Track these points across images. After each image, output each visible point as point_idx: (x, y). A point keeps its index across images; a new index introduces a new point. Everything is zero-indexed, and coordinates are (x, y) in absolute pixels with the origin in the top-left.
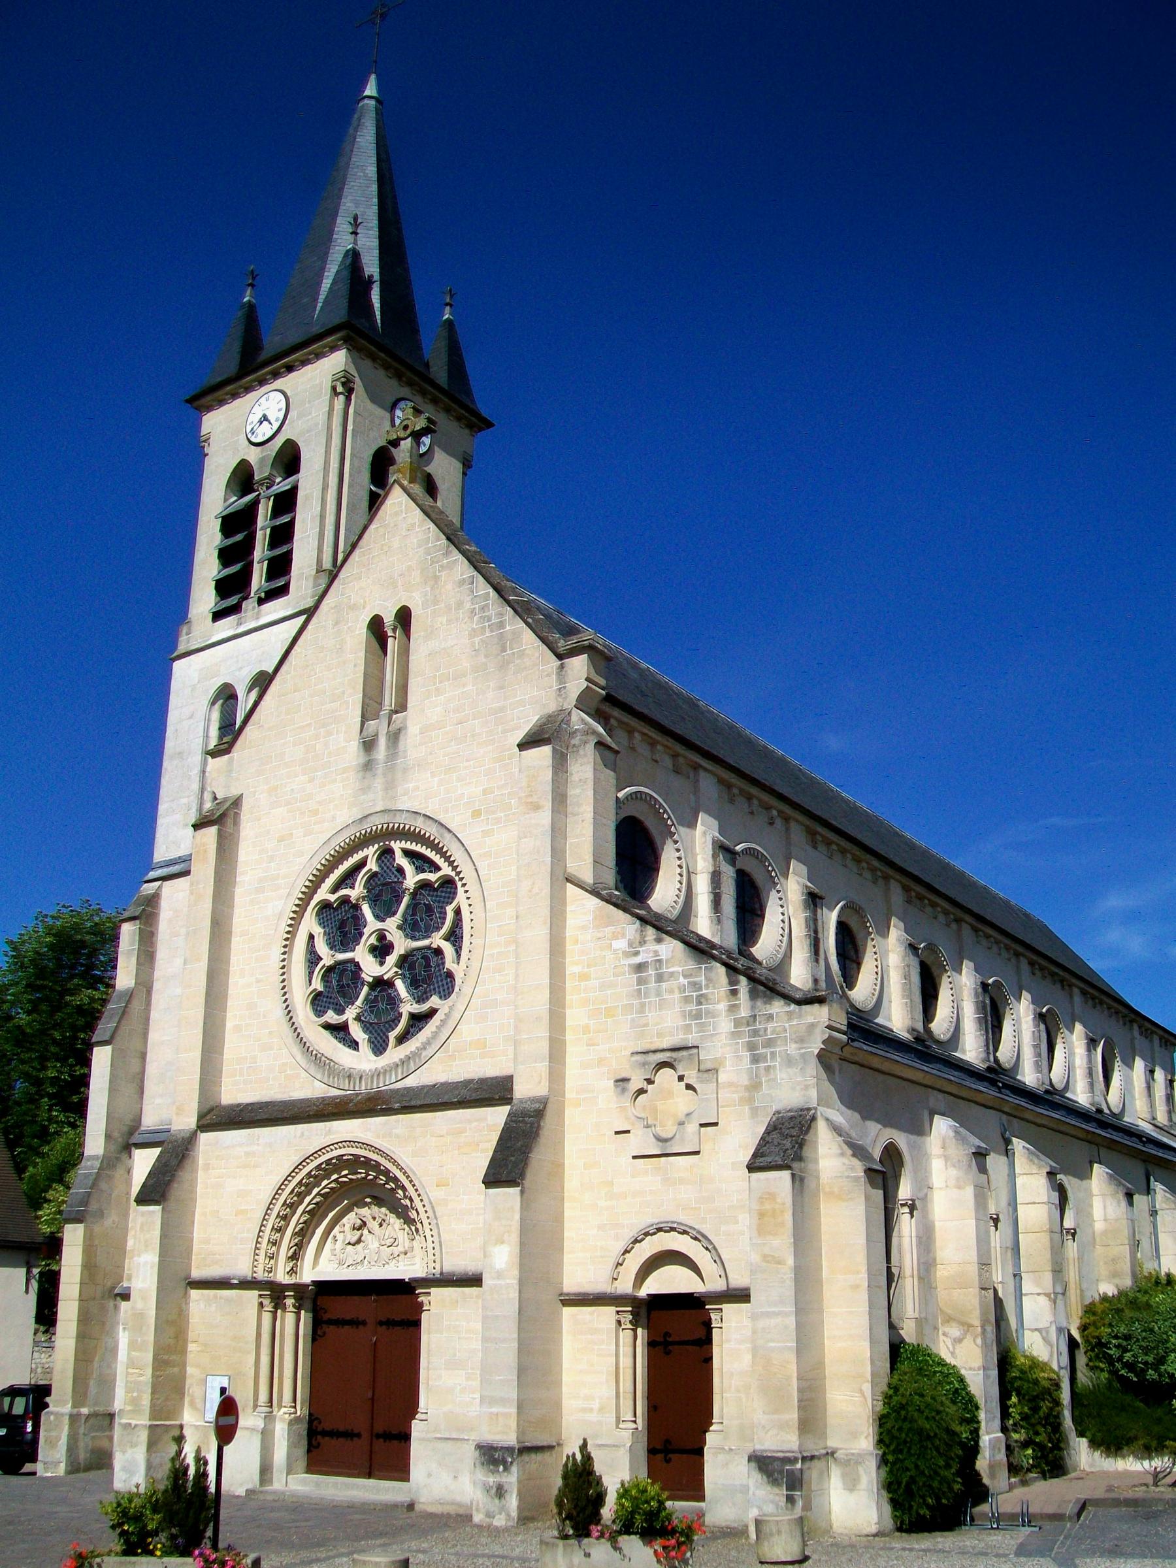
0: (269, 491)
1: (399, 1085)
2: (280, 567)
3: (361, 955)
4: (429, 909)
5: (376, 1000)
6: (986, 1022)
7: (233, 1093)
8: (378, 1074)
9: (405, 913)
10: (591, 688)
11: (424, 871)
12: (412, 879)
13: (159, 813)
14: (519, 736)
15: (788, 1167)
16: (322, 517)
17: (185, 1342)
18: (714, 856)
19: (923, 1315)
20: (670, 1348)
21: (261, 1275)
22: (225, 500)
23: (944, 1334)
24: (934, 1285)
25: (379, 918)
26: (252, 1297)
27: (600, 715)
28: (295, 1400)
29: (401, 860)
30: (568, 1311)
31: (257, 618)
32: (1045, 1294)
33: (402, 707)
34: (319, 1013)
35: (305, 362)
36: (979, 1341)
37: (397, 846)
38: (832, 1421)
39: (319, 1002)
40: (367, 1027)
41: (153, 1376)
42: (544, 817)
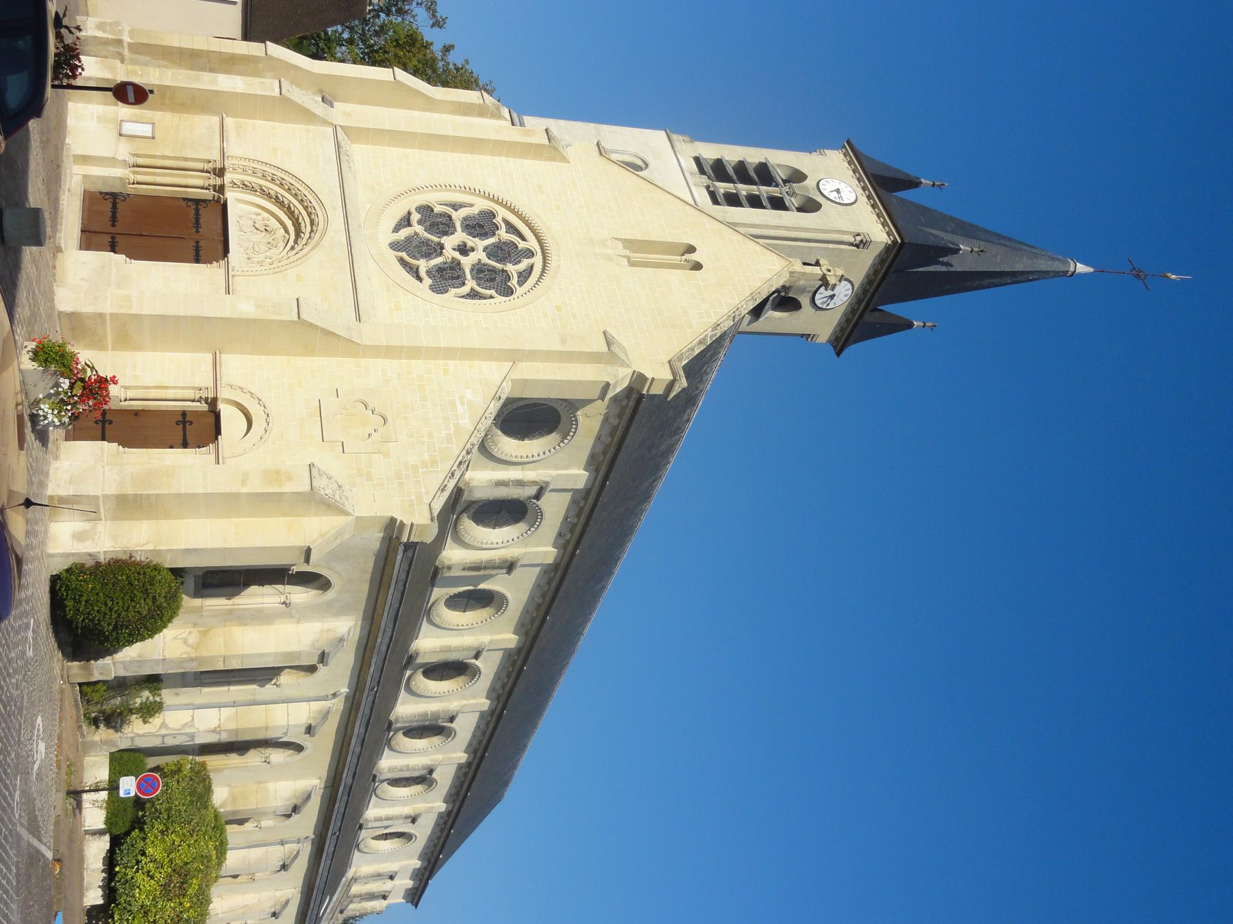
0: (786, 194)
2: (733, 200)
3: (459, 236)
4: (492, 280)
5: (428, 245)
6: (424, 720)
7: (358, 152)
9: (490, 266)
11: (519, 277)
12: (512, 269)
13: (557, 120)
16: (767, 227)
18: (534, 483)
19: (205, 614)
20: (181, 426)
22: (778, 165)
23: (190, 632)
24: (227, 623)
25: (485, 249)
27: (629, 391)
28: (138, 183)
29: (525, 264)
31: (695, 185)
32: (219, 725)
33: (633, 264)
34: (419, 209)
36: (185, 656)
37: (537, 260)
38: (126, 525)
39: (426, 210)
40: (409, 240)
42: (556, 346)
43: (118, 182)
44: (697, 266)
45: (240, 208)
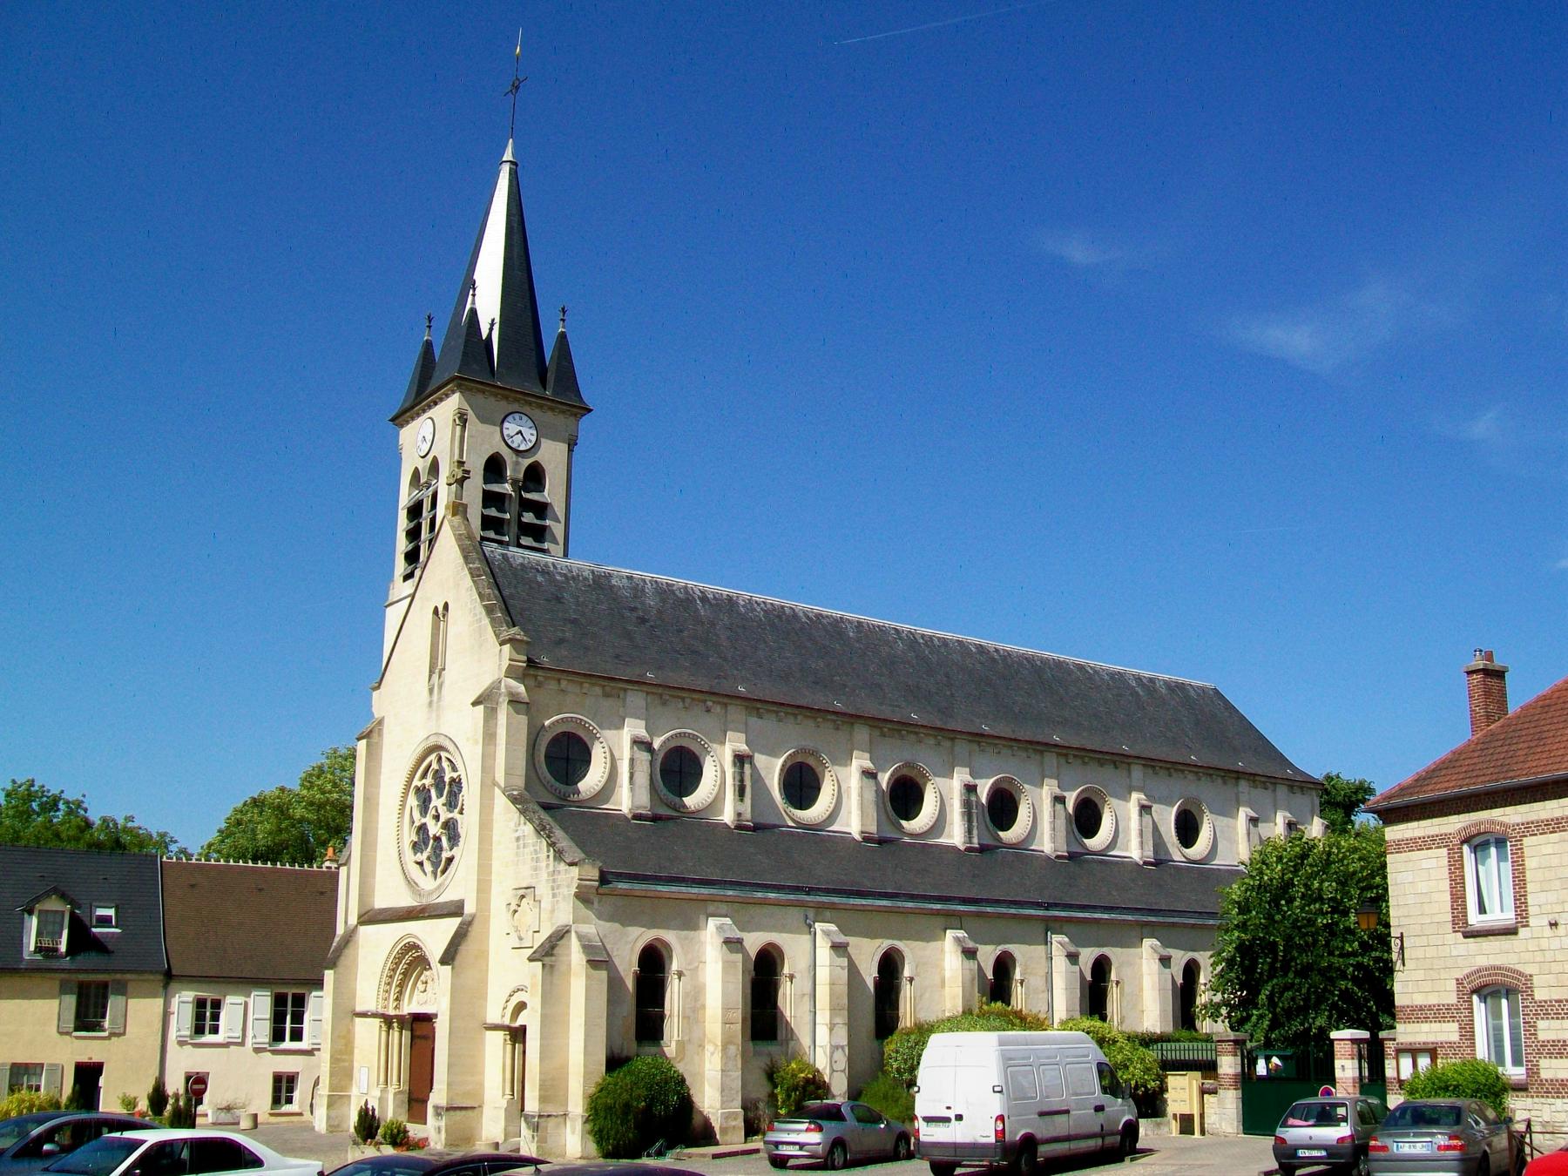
1: (437, 901)
7: (381, 902)
8: (431, 893)
10: (513, 665)
14: (473, 699)
15: (541, 961)
17: (353, 1048)
21: (381, 1011)
22: (409, 495)
26: (377, 1021)
28: (399, 1081)
29: (445, 764)
30: (488, 1033)
35: (441, 400)
39: (416, 847)
41: (331, 1067)
43: (398, 1096)
44: (446, 606)
45: (410, 1007)
